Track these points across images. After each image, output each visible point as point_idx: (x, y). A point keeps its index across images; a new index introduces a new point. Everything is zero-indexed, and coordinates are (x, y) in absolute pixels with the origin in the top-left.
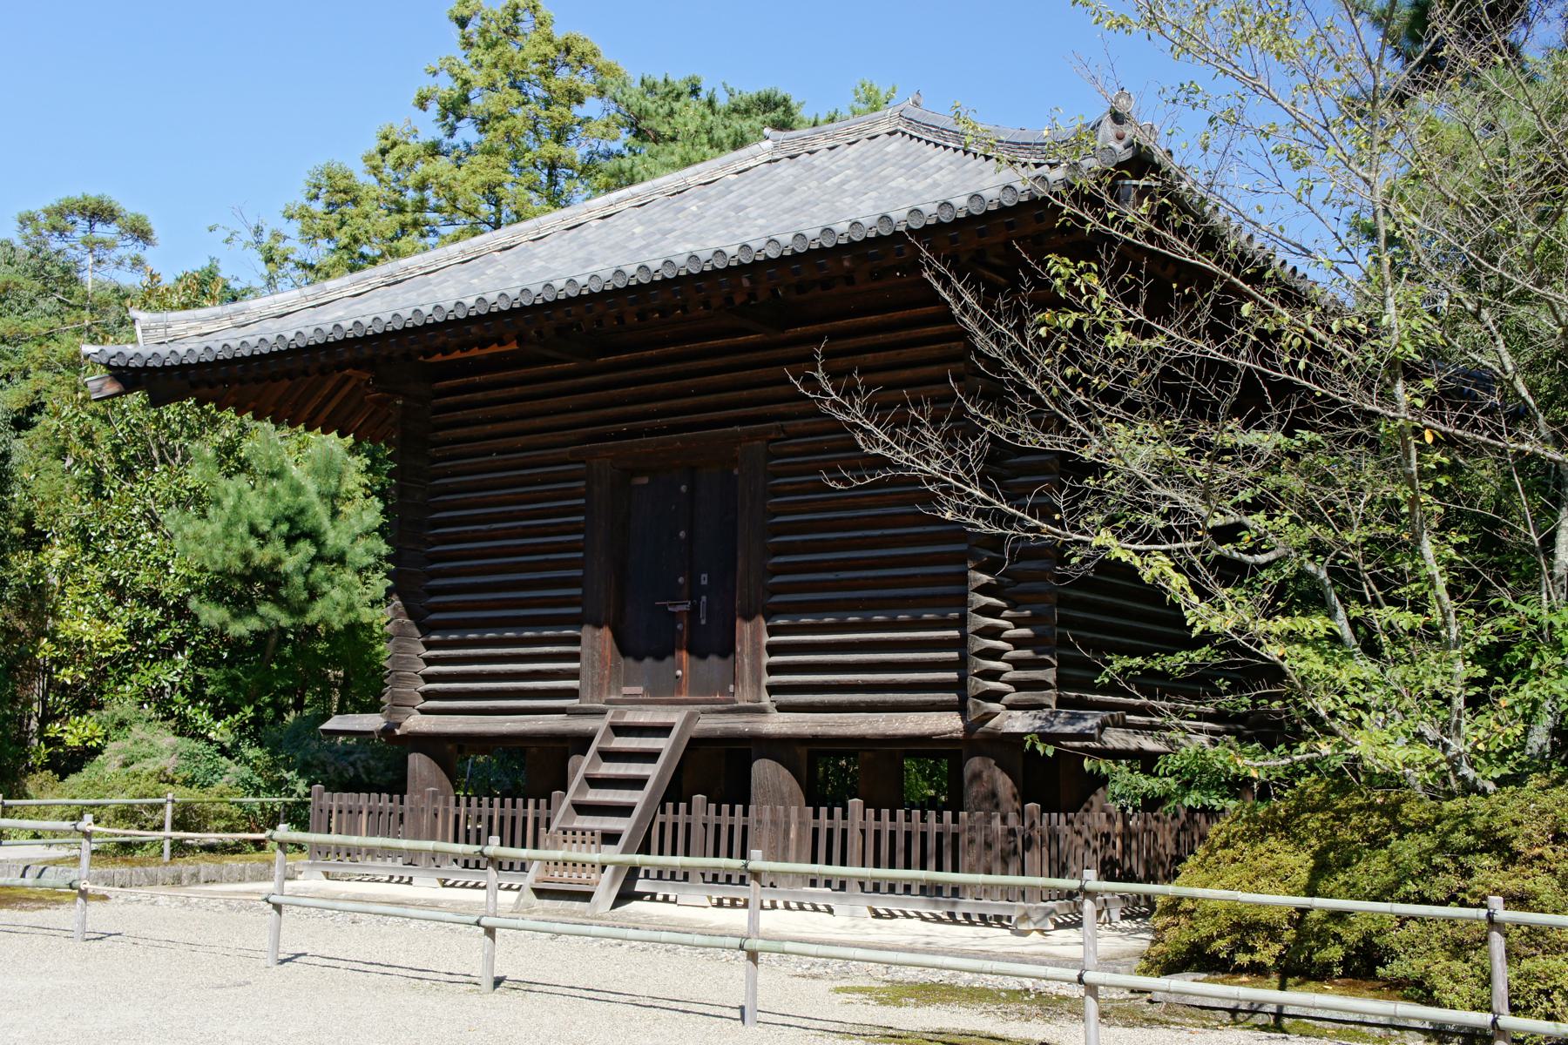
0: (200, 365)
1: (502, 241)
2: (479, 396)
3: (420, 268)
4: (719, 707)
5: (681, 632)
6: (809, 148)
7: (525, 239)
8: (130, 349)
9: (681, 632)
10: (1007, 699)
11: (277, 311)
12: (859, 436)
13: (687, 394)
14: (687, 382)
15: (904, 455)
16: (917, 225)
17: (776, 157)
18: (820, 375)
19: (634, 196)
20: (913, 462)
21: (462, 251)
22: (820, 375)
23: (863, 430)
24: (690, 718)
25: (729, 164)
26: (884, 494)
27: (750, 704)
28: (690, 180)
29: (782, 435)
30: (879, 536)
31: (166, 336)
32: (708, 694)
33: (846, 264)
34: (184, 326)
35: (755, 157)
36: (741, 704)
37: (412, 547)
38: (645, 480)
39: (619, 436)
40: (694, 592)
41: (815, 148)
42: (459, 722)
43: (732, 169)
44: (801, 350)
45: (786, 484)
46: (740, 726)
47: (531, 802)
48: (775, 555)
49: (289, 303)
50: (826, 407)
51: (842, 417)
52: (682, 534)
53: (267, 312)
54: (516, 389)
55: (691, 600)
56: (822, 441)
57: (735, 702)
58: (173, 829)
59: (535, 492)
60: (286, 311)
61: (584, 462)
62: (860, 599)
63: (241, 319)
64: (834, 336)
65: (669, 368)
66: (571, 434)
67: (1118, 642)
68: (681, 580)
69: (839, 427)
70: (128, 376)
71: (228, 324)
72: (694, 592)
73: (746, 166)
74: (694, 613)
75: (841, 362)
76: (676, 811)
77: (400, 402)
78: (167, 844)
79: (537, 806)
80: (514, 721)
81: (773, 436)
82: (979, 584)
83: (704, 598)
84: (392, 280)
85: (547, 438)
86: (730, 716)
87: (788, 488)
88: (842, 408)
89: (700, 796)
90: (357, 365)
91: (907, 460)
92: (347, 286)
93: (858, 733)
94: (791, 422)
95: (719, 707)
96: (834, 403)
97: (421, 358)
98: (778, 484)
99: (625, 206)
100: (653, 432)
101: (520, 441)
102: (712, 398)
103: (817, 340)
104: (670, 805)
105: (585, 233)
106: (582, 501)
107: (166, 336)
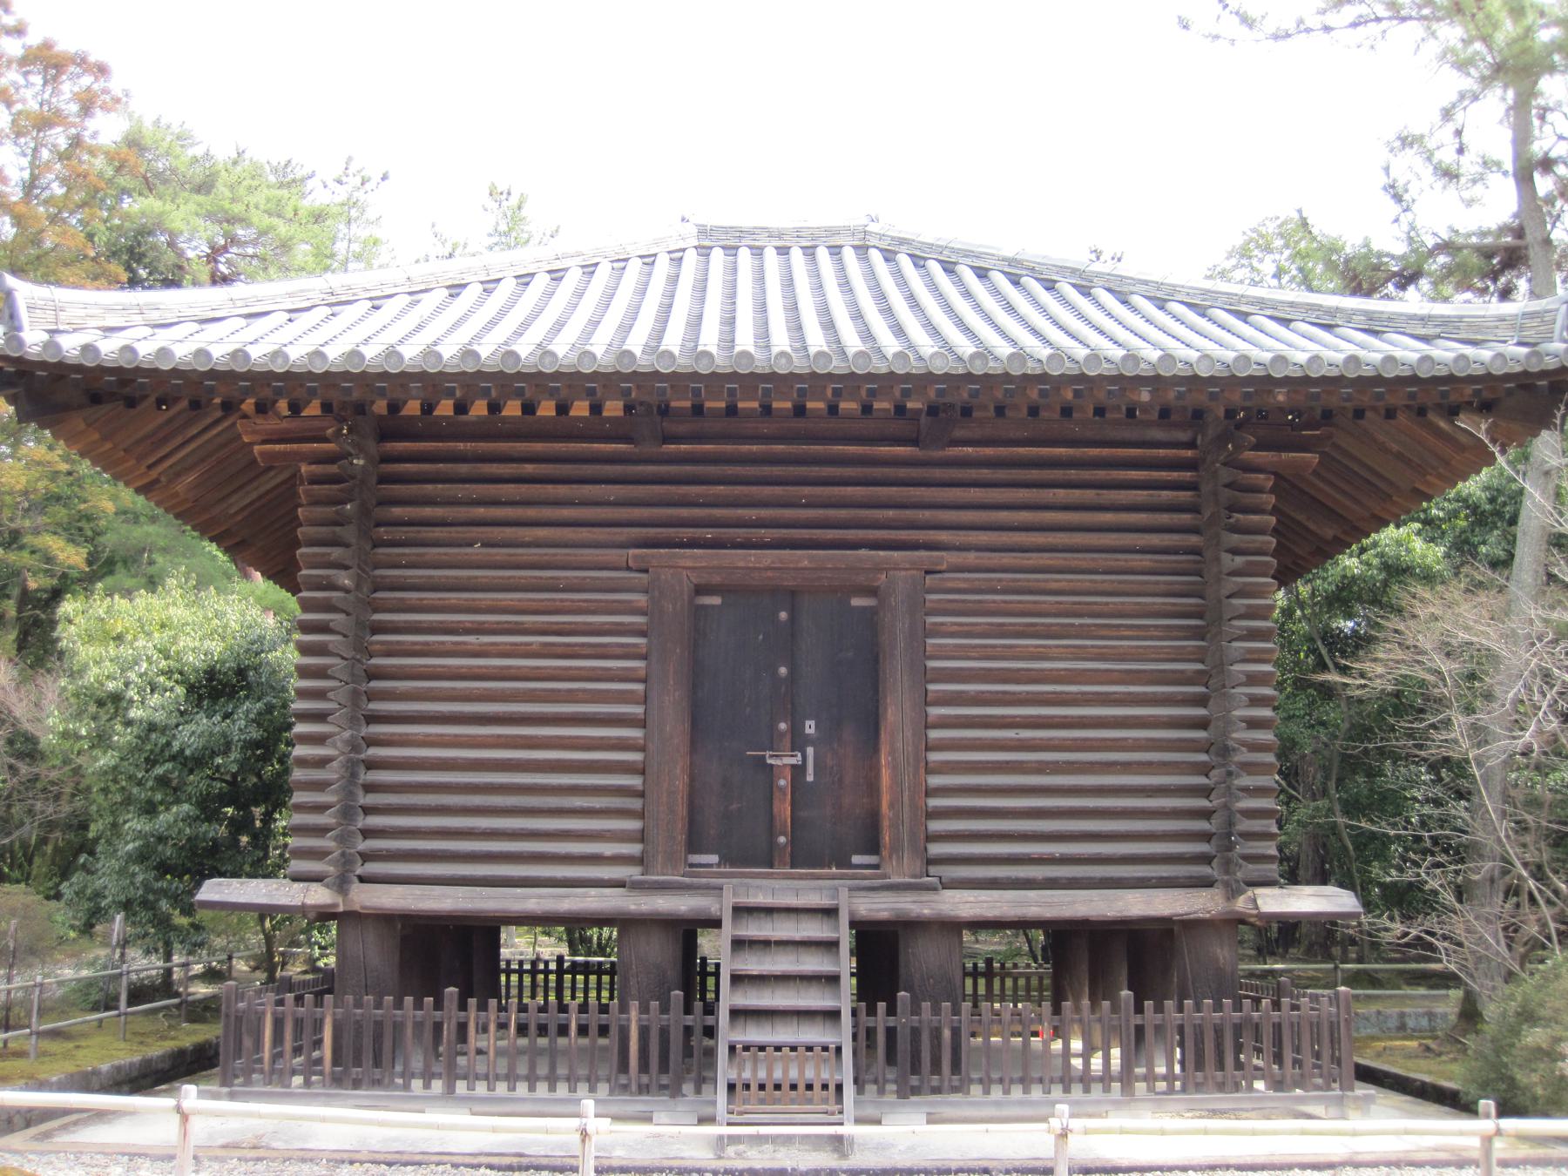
1: (451, 275)
4: (866, 883)
26: (1086, 647)
27: (907, 880)
33: (1281, 398)
36: (896, 879)
57: (885, 876)
59: (562, 600)
80: (540, 897)
83: (810, 751)
84: (333, 299)
86: (885, 893)
95: (866, 883)
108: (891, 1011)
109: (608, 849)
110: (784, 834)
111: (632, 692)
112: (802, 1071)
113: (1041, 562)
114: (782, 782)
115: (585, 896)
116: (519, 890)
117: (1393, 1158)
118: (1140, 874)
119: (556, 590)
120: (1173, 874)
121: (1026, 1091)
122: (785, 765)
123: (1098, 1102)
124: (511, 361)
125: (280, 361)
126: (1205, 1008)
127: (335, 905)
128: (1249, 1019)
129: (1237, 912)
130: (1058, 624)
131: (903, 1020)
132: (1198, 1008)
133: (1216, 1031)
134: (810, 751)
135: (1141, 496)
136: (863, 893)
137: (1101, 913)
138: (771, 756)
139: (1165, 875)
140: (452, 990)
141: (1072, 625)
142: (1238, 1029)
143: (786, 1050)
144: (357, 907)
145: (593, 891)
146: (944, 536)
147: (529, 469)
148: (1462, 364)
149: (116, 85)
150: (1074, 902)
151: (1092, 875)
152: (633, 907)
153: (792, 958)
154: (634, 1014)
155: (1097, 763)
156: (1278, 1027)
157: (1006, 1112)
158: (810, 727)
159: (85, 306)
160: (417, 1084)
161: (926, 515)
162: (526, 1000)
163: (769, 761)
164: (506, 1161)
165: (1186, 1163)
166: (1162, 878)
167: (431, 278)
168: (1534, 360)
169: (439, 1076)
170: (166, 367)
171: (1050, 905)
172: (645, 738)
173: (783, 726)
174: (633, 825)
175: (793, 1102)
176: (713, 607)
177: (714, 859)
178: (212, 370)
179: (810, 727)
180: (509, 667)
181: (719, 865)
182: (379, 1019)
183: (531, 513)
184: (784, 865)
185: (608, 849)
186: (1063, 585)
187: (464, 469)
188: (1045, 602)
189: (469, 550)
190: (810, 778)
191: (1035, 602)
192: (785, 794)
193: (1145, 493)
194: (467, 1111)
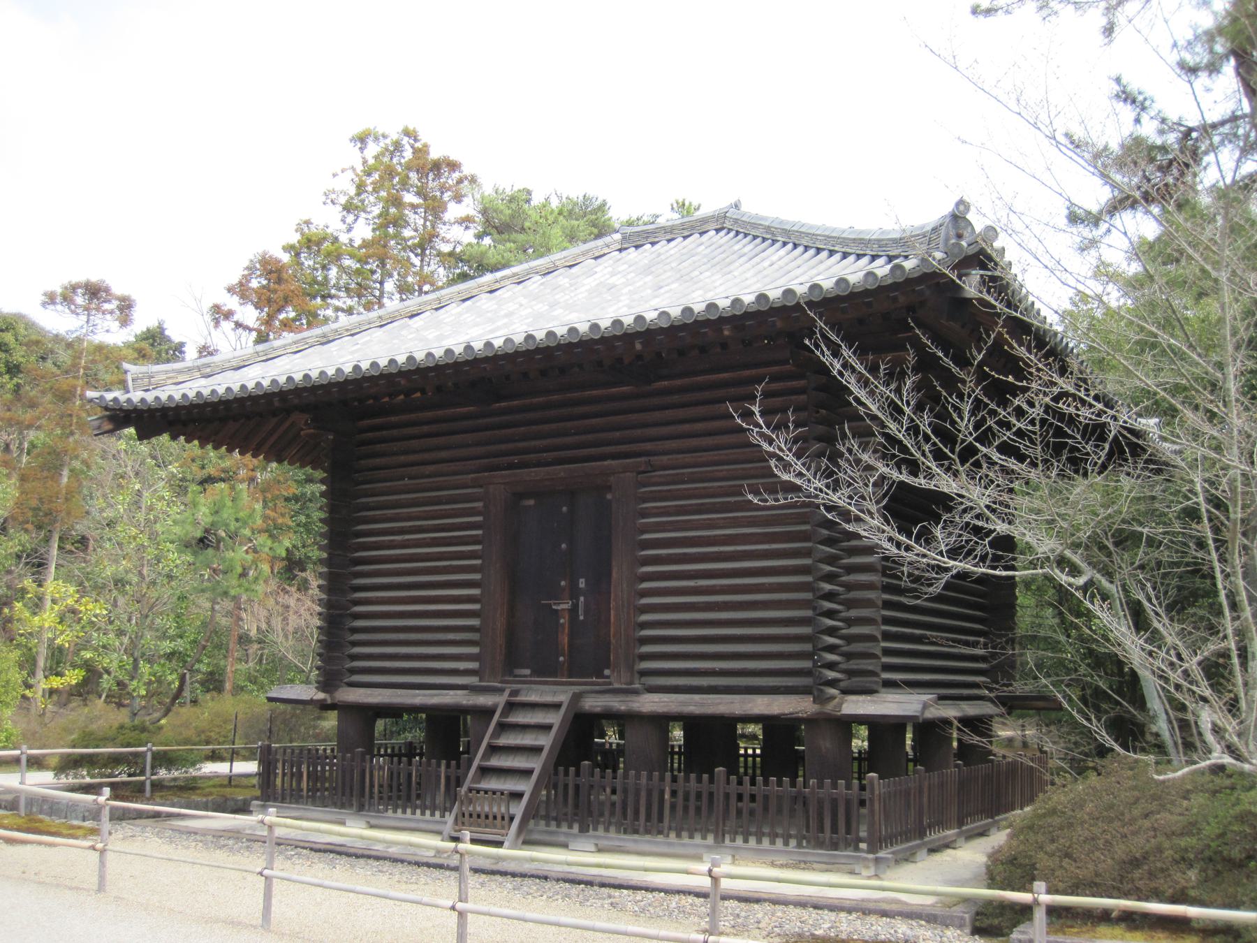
0: (179, 408)
1: (412, 309)
2: (395, 432)
3: (347, 330)
4: (597, 688)
6: (651, 240)
9: (563, 625)
10: (842, 684)
12: (773, 462)
13: (566, 434)
16: (816, 298)
19: (514, 275)
21: (380, 317)
23: (780, 459)
24: (576, 698)
25: (588, 251)
27: (624, 686)
28: (558, 263)
29: (650, 469)
33: (726, 333)
34: (164, 377)
35: (608, 246)
36: (616, 686)
37: (340, 552)
38: (531, 502)
39: (511, 466)
40: (574, 593)
41: (656, 240)
42: (379, 695)
46: (616, 704)
47: (444, 762)
49: (244, 358)
50: (755, 438)
52: (564, 546)
53: (227, 365)
57: (610, 684)
58: (1142, 534)
60: (242, 364)
63: (208, 370)
64: (774, 379)
68: (563, 583)
71: (198, 374)
72: (574, 593)
73: (602, 253)
74: (574, 611)
75: (777, 401)
76: (566, 774)
79: (448, 766)
80: (425, 695)
82: (822, 593)
83: (582, 599)
84: (325, 340)
86: (607, 695)
87: (655, 511)
90: (303, 409)
92: (290, 345)
94: (656, 458)
95: (597, 688)
96: (762, 435)
100: (539, 464)
102: (590, 437)
104: (561, 769)
105: (478, 304)
107: (150, 384)
108: (578, 774)
112: (491, 808)
114: (562, 621)
115: (447, 695)
120: (795, 684)
122: (563, 610)
123: (698, 846)
125: (531, 342)
126: (784, 785)
127: (325, 700)
128: (799, 792)
131: (583, 780)
132: (821, 785)
133: (819, 802)
134: (582, 599)
135: (469, 438)
136: (593, 695)
137: (732, 711)
138: (555, 604)
139: (790, 684)
140: (720, 770)
141: (729, 502)
143: (482, 793)
144: (336, 701)
145: (451, 692)
146: (648, 446)
149: (467, 170)
150: (720, 704)
151: (740, 684)
152: (464, 702)
153: (533, 736)
156: (780, 798)
157: (671, 850)
158: (582, 583)
159: (167, 372)
160: (779, 842)
161: (638, 432)
162: (676, 773)
163: (554, 607)
164: (322, 847)
168: (898, 272)
169: (712, 831)
170: (231, 398)
172: (482, 594)
173: (563, 583)
175: (486, 826)
176: (530, 506)
177: (528, 672)
178: (746, 312)
179: (582, 583)
181: (531, 676)
182: (835, 796)
183: (426, 456)
184: (562, 676)
190: (581, 618)
193: (780, 399)
194: (363, 824)
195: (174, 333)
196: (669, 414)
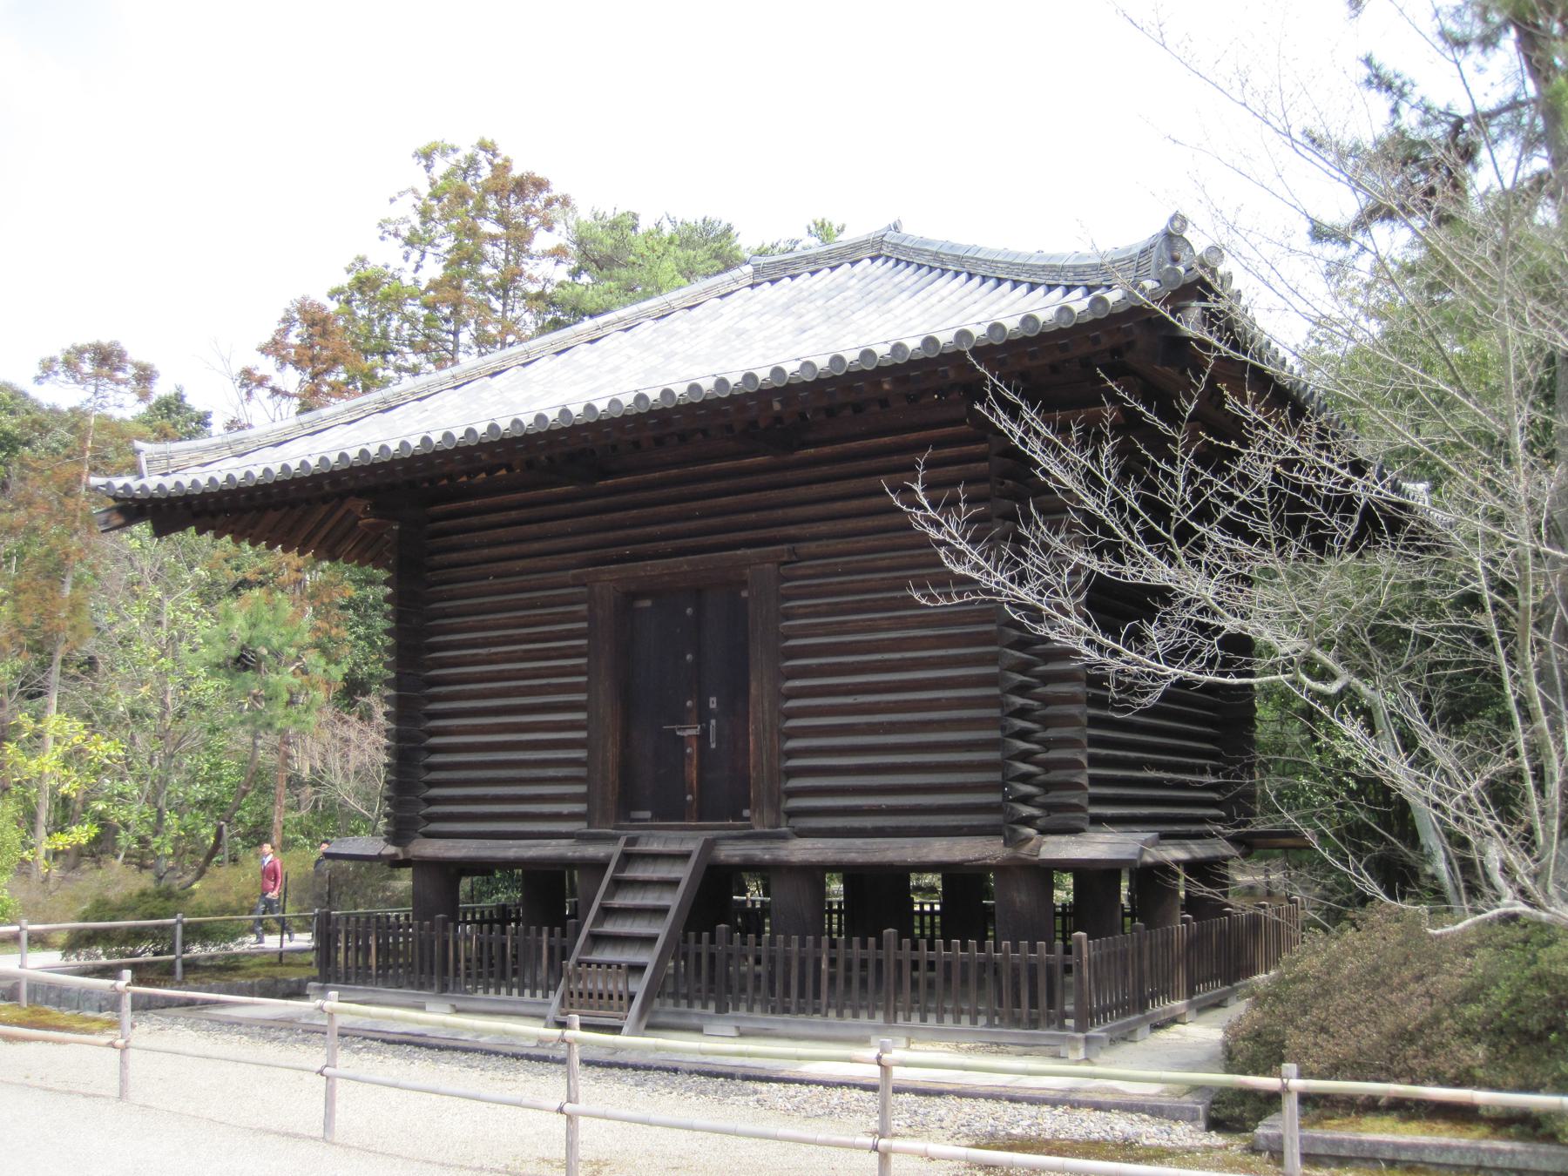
1: (493, 365)
3: (413, 393)
4: (735, 833)
5: (690, 756)
7: (514, 363)
8: (134, 483)
9: (690, 756)
11: (274, 439)
14: (693, 505)
15: (997, 578)
17: (758, 281)
18: (918, 488)
19: (620, 320)
20: (1004, 586)
22: (918, 488)
24: (709, 845)
25: (712, 288)
26: (905, 617)
27: (767, 830)
29: (794, 558)
30: (900, 660)
31: (169, 466)
32: (722, 820)
35: (737, 282)
36: (758, 829)
38: (647, 603)
40: (703, 715)
41: (797, 272)
42: (464, 847)
43: (715, 293)
44: (905, 459)
45: (800, 607)
46: (758, 853)
48: (788, 679)
49: (286, 431)
51: (933, 533)
54: (513, 513)
55: (700, 723)
56: (836, 564)
57: (751, 827)
59: (535, 616)
60: (283, 439)
61: (585, 585)
62: (881, 724)
63: (241, 447)
64: (938, 444)
65: (673, 491)
66: (570, 558)
67: (1126, 757)
68: (689, 703)
69: (925, 543)
70: (133, 509)
72: (703, 715)
74: (703, 737)
77: (396, 527)
78: (179, 928)
80: (520, 847)
81: (785, 559)
82: (1012, 709)
83: (713, 722)
84: (386, 406)
85: (548, 561)
86: (747, 842)
88: (938, 525)
89: (723, 926)
90: (360, 493)
91: (997, 583)
92: (342, 413)
93: (886, 860)
95: (735, 833)
97: (464, 479)
98: (792, 607)
99: (611, 329)
101: (519, 565)
103: (920, 447)
104: (692, 934)
105: (576, 357)
106: (584, 625)
107: (169, 466)
108: (712, 940)
109: (565, 808)
110: (691, 793)
111: (578, 684)
113: (870, 543)
115: (547, 846)
116: (511, 842)
117: (921, 1086)
118: (955, 823)
119: (535, 607)
120: (982, 823)
121: (676, 1004)
122: (690, 736)
123: (863, 1026)
124: (1065, 316)
125: (472, 436)
126: (1022, 949)
127: (396, 855)
128: (989, 958)
129: (1021, 859)
130: (882, 599)
132: (1016, 949)
139: (975, 823)
141: (895, 598)
142: (982, 966)
145: (554, 842)
147: (514, 514)
148: (998, 333)
152: (570, 854)
154: (545, 936)
155: (989, 718)
158: (713, 703)
159: (189, 451)
162: (835, 936)
164: (397, 1038)
165: (270, 1051)
166: (972, 826)
167: (474, 372)
168: (1099, 307)
171: (865, 851)
174: (581, 789)
177: (648, 814)
178: (910, 361)
179: (713, 703)
180: (503, 671)
185: (565, 808)
186: (885, 563)
187: (475, 520)
188: (871, 580)
189: (485, 582)
191: (863, 581)
192: (692, 760)
193: (956, 468)
195: (196, 401)
196: (817, 490)
